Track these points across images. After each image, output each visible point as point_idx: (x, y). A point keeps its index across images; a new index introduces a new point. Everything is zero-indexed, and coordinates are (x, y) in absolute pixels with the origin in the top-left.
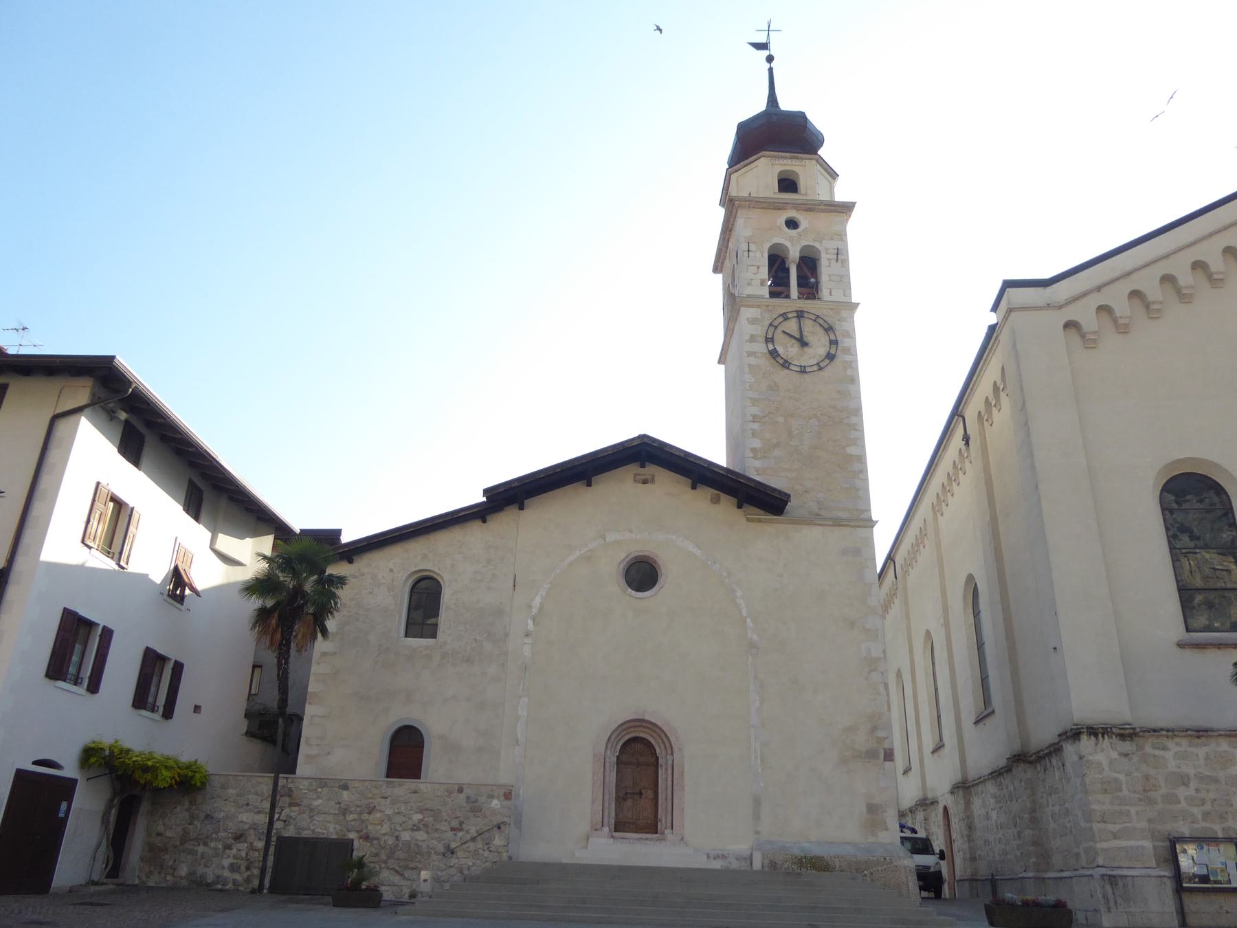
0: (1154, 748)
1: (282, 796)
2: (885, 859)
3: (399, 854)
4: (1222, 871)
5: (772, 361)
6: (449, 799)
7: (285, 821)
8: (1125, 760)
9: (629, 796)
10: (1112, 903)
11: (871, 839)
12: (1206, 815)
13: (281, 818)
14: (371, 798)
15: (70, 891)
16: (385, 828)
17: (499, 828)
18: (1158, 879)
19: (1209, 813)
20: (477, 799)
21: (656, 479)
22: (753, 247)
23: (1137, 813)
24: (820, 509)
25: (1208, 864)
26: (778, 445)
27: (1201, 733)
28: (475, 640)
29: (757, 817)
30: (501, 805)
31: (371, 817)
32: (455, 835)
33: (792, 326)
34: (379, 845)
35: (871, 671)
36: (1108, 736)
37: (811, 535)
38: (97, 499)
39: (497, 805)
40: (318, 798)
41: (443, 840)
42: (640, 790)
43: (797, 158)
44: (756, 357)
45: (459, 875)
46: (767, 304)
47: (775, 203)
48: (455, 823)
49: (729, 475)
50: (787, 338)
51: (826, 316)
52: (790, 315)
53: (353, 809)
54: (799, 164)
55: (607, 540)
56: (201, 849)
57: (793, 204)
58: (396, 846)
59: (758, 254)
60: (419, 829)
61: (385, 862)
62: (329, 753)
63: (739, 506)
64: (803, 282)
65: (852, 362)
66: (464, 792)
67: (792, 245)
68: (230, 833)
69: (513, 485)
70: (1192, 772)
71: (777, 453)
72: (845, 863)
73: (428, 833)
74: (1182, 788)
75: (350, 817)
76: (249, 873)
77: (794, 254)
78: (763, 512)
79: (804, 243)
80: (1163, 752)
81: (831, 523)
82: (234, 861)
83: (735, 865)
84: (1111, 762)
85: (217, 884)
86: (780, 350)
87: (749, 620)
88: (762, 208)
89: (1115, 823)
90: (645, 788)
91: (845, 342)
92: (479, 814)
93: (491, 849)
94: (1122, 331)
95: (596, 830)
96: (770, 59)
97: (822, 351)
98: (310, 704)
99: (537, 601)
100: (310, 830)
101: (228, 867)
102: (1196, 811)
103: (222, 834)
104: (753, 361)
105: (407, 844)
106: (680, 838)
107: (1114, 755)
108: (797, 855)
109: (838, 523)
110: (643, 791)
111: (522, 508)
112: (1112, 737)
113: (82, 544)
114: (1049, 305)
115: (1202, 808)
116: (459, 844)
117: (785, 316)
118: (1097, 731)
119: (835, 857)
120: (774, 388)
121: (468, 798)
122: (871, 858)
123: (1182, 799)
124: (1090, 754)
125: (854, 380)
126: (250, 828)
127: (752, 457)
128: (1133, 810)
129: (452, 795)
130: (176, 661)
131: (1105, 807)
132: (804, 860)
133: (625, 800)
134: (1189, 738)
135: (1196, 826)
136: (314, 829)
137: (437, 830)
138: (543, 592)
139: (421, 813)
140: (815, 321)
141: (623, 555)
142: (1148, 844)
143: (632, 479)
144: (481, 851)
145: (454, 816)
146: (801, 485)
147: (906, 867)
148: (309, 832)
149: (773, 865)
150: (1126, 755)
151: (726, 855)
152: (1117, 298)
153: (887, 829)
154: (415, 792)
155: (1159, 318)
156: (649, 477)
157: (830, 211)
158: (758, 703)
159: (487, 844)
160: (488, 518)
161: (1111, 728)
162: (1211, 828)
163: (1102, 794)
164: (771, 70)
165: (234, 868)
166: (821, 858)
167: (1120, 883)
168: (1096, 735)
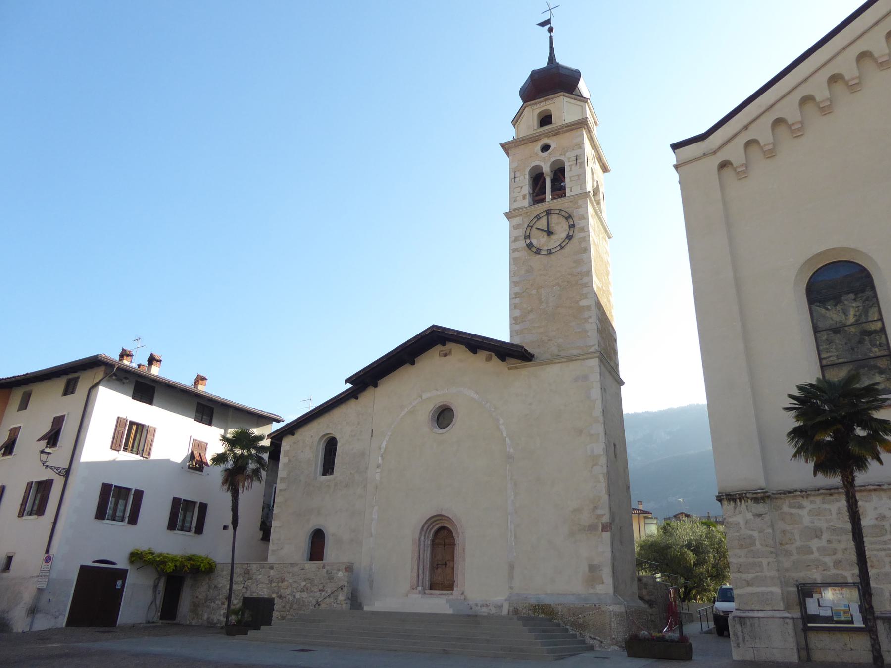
0: (790, 506)
2: (595, 605)
4: (845, 612)
5: (529, 251)
7: (246, 588)
8: (758, 519)
9: (439, 566)
10: (741, 639)
11: (591, 591)
12: (837, 563)
15: (134, 627)
16: (288, 591)
18: (781, 619)
19: (840, 561)
20: (331, 572)
21: (452, 353)
22: (518, 174)
23: (768, 563)
25: (832, 606)
26: (531, 311)
27: (832, 491)
28: (351, 473)
29: (511, 577)
31: (283, 584)
33: (542, 224)
36: (745, 501)
37: (551, 372)
38: (118, 426)
40: (260, 574)
41: (315, 597)
43: (549, 99)
46: (526, 212)
48: (321, 587)
49: (484, 341)
50: (540, 232)
51: (568, 208)
52: (542, 215)
54: (552, 102)
55: (423, 398)
56: (213, 604)
57: (544, 134)
59: (522, 178)
60: (304, 591)
61: (289, 611)
65: (585, 237)
67: (545, 163)
69: (360, 374)
70: (823, 525)
72: (565, 609)
73: (308, 593)
74: (816, 540)
75: (274, 585)
77: (547, 169)
78: (520, 361)
79: (553, 159)
80: (798, 510)
81: (565, 360)
83: (493, 611)
84: (747, 522)
85: (218, 624)
86: (534, 242)
89: (749, 573)
90: (448, 560)
91: (579, 224)
92: (332, 581)
93: (338, 602)
95: (413, 589)
96: (551, 30)
102: (828, 560)
103: (221, 596)
105: (298, 599)
106: (461, 592)
107: (749, 516)
110: (448, 562)
112: (748, 501)
113: (111, 450)
115: (834, 557)
117: (538, 217)
118: (734, 497)
120: (530, 270)
121: (327, 571)
122: (585, 605)
123: (815, 549)
124: (730, 517)
127: (514, 323)
128: (765, 561)
131: (741, 560)
132: (537, 607)
133: (437, 568)
134: (822, 496)
135: (829, 573)
137: (312, 592)
138: (387, 438)
140: (559, 214)
141: (432, 406)
142: (777, 590)
143: (438, 355)
144: (332, 603)
146: (547, 336)
149: (516, 611)
150: (760, 515)
151: (488, 604)
152: (762, 132)
153: (603, 583)
154: (302, 569)
155: (802, 135)
156: (448, 352)
157: (572, 130)
158: (512, 497)
160: (359, 396)
161: (746, 494)
162: (842, 575)
163: (739, 549)
164: (551, 37)
166: (549, 606)
167: (749, 624)
168: (734, 500)
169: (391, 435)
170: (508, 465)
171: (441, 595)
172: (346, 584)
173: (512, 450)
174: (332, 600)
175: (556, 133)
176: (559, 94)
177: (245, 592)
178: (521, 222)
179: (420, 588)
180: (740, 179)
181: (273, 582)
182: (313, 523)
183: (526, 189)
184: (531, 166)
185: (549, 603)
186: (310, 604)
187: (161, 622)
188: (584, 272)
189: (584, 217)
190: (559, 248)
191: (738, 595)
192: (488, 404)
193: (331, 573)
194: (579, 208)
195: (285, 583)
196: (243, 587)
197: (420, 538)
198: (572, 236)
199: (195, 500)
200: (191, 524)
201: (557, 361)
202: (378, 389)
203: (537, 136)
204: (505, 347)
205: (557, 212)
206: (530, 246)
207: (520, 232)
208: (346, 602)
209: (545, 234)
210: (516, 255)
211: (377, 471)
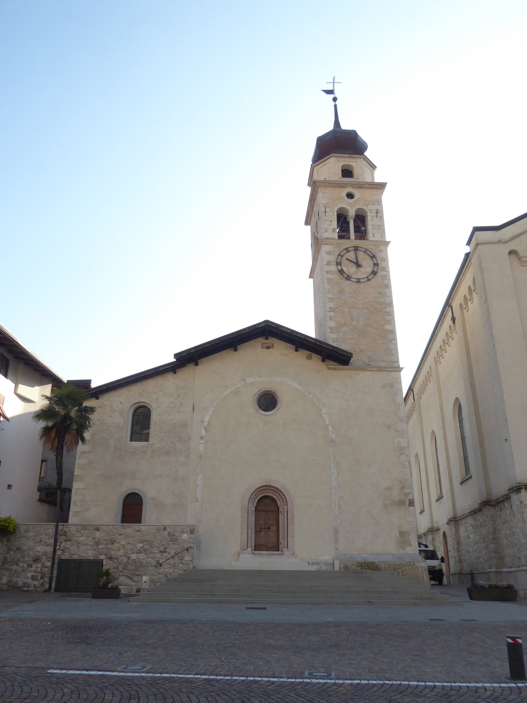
1: (61, 536)
2: (410, 563)
3: (130, 567)
7: (62, 550)
9: (262, 529)
11: (402, 551)
13: (60, 549)
16: (121, 552)
24: (370, 361)
26: (345, 324)
29: (336, 540)
33: (351, 255)
34: (118, 562)
35: (401, 454)
37: (365, 377)
39: (186, 537)
42: (269, 526)
44: (331, 274)
45: (165, 578)
46: (336, 243)
48: (162, 548)
51: (371, 249)
56: (14, 567)
57: (351, 184)
58: (128, 562)
59: (331, 214)
60: (141, 552)
61: (122, 572)
63: (323, 361)
66: (167, 530)
69: (191, 351)
75: (100, 547)
76: (42, 580)
77: (352, 213)
78: (337, 364)
79: (358, 207)
82: (34, 574)
83: (324, 568)
85: (25, 587)
86: (345, 269)
87: (330, 426)
90: (271, 525)
91: (382, 265)
96: (335, 99)
97: (369, 270)
98: (76, 482)
99: (207, 418)
100: (78, 555)
104: (329, 276)
105: (134, 561)
108: (360, 562)
109: (380, 369)
110: (270, 527)
111: (197, 364)
114: (500, 241)
116: (165, 560)
117: (347, 250)
120: (342, 291)
121: (169, 533)
122: (402, 562)
125: (388, 286)
126: (42, 555)
129: (160, 532)
132: (364, 564)
133: (260, 532)
138: (210, 413)
140: (365, 252)
145: (161, 544)
147: (422, 567)
149: (346, 567)
151: (319, 562)
153: (411, 545)
156: (271, 345)
157: (372, 188)
158: (336, 475)
159: (181, 560)
160: (177, 371)
164: (335, 106)
165: (33, 578)
169: (214, 411)
170: (331, 448)
174: (177, 561)
175: (360, 186)
176: (330, 155)
177: (62, 554)
178: (332, 250)
180: (522, 266)
181: (99, 544)
182: (128, 487)
184: (339, 207)
185: (373, 561)
188: (387, 303)
192: (311, 395)
193: (174, 535)
194: (381, 252)
198: (377, 272)
201: (369, 369)
202: (198, 368)
203: (346, 184)
204: (213, 344)
205: (364, 250)
209: (354, 266)
211: (201, 442)
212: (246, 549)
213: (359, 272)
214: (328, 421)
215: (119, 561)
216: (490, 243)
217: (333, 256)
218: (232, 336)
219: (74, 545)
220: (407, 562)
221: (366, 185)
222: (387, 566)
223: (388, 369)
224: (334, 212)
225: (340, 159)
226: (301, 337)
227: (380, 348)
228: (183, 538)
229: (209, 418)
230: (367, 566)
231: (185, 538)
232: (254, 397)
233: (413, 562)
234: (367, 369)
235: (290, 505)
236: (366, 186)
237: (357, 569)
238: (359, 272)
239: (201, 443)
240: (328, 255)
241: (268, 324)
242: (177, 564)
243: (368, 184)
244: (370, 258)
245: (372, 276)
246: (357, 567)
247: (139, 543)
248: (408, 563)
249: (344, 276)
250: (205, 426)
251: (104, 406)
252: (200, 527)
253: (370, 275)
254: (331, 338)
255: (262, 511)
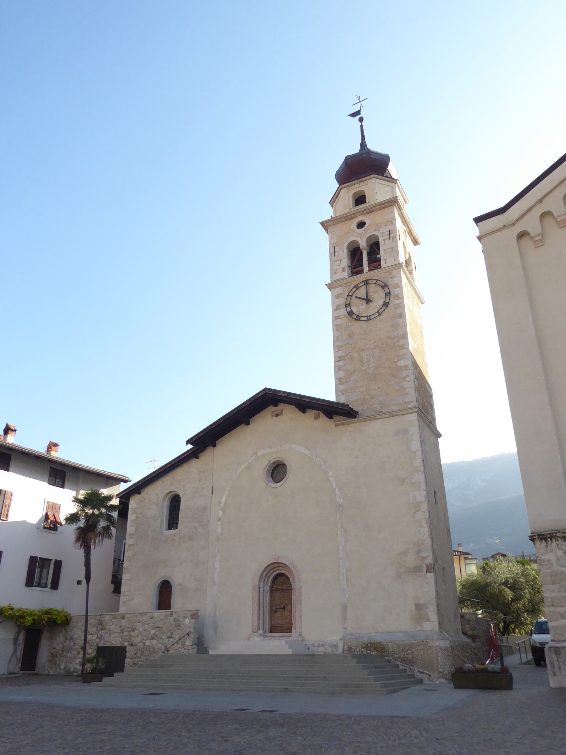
2: (423, 641)
6: (167, 620)
7: (100, 638)
11: (418, 628)
14: (134, 623)
16: (139, 639)
17: (188, 635)
21: (284, 412)
24: (381, 408)
26: (354, 372)
30: (189, 622)
31: (134, 633)
32: (169, 640)
33: (361, 292)
35: (417, 511)
36: (555, 539)
40: (113, 625)
41: (164, 644)
42: (284, 606)
44: (340, 319)
47: (347, 216)
48: (169, 634)
50: (359, 300)
51: (383, 278)
53: (126, 629)
56: (69, 655)
59: (341, 252)
60: (153, 639)
62: (132, 600)
64: (370, 262)
66: (173, 616)
68: (79, 646)
69: (200, 435)
71: (354, 377)
73: (157, 640)
75: (125, 634)
77: (363, 244)
78: (345, 418)
79: (368, 235)
83: (329, 650)
84: (558, 559)
86: (354, 309)
88: (342, 222)
90: (286, 605)
91: (395, 292)
92: (179, 628)
93: (184, 648)
94: (563, 226)
96: (361, 120)
97: (381, 302)
100: (110, 642)
101: (79, 664)
106: (299, 634)
108: (365, 642)
110: (286, 606)
111: (215, 446)
112: (558, 540)
114: (504, 226)
117: (357, 287)
119: (389, 642)
121: (175, 619)
122: (413, 641)
130: (56, 560)
131: (554, 594)
132: (369, 645)
133: (276, 612)
136: (111, 642)
138: (226, 493)
139: (154, 629)
140: (375, 284)
145: (169, 630)
147: (437, 647)
148: (109, 643)
149: (350, 649)
151: (324, 644)
153: (429, 621)
154: (152, 618)
156: (279, 412)
158: (343, 544)
160: (200, 455)
161: (556, 533)
164: (362, 126)
168: (546, 539)
170: (338, 514)
171: (281, 637)
172: (192, 630)
173: (341, 500)
175: (370, 211)
179: (261, 632)
180: (537, 247)
183: (345, 262)
184: (349, 241)
186: (160, 650)
187: (22, 672)
189: (399, 286)
190: (377, 314)
191: (552, 627)
192: (318, 459)
193: (178, 621)
194: (393, 278)
195: (136, 632)
196: (97, 637)
197: (259, 585)
199: (50, 558)
200: (47, 581)
201: (379, 417)
203: (353, 214)
206: (351, 313)
207: (342, 301)
208: (193, 647)
209: (364, 302)
210: (339, 322)
211: (218, 524)
212: (257, 631)
213: (370, 308)
214: (335, 484)
215: (137, 648)
216: (493, 233)
217: (342, 298)
218: (235, 412)
219: (107, 633)
220: (419, 641)
221: (377, 207)
222: (396, 646)
223: (401, 413)
224: (343, 249)
225: (350, 188)
226: (297, 398)
227: (393, 390)
228: (185, 623)
229: (225, 498)
230: (373, 646)
231: (187, 623)
232: (264, 470)
233: (426, 641)
234: (377, 417)
235: (297, 582)
236: (375, 208)
237: (362, 651)
238: (370, 308)
239: (218, 525)
240: (338, 298)
241: (266, 392)
242: (180, 649)
243: (377, 205)
244: (382, 289)
245: (384, 308)
246: (362, 648)
247: (152, 630)
248: (420, 642)
249: (353, 318)
250: (222, 507)
251: (145, 499)
252: (217, 611)
253: (381, 308)
254: (340, 390)
255: (278, 590)
